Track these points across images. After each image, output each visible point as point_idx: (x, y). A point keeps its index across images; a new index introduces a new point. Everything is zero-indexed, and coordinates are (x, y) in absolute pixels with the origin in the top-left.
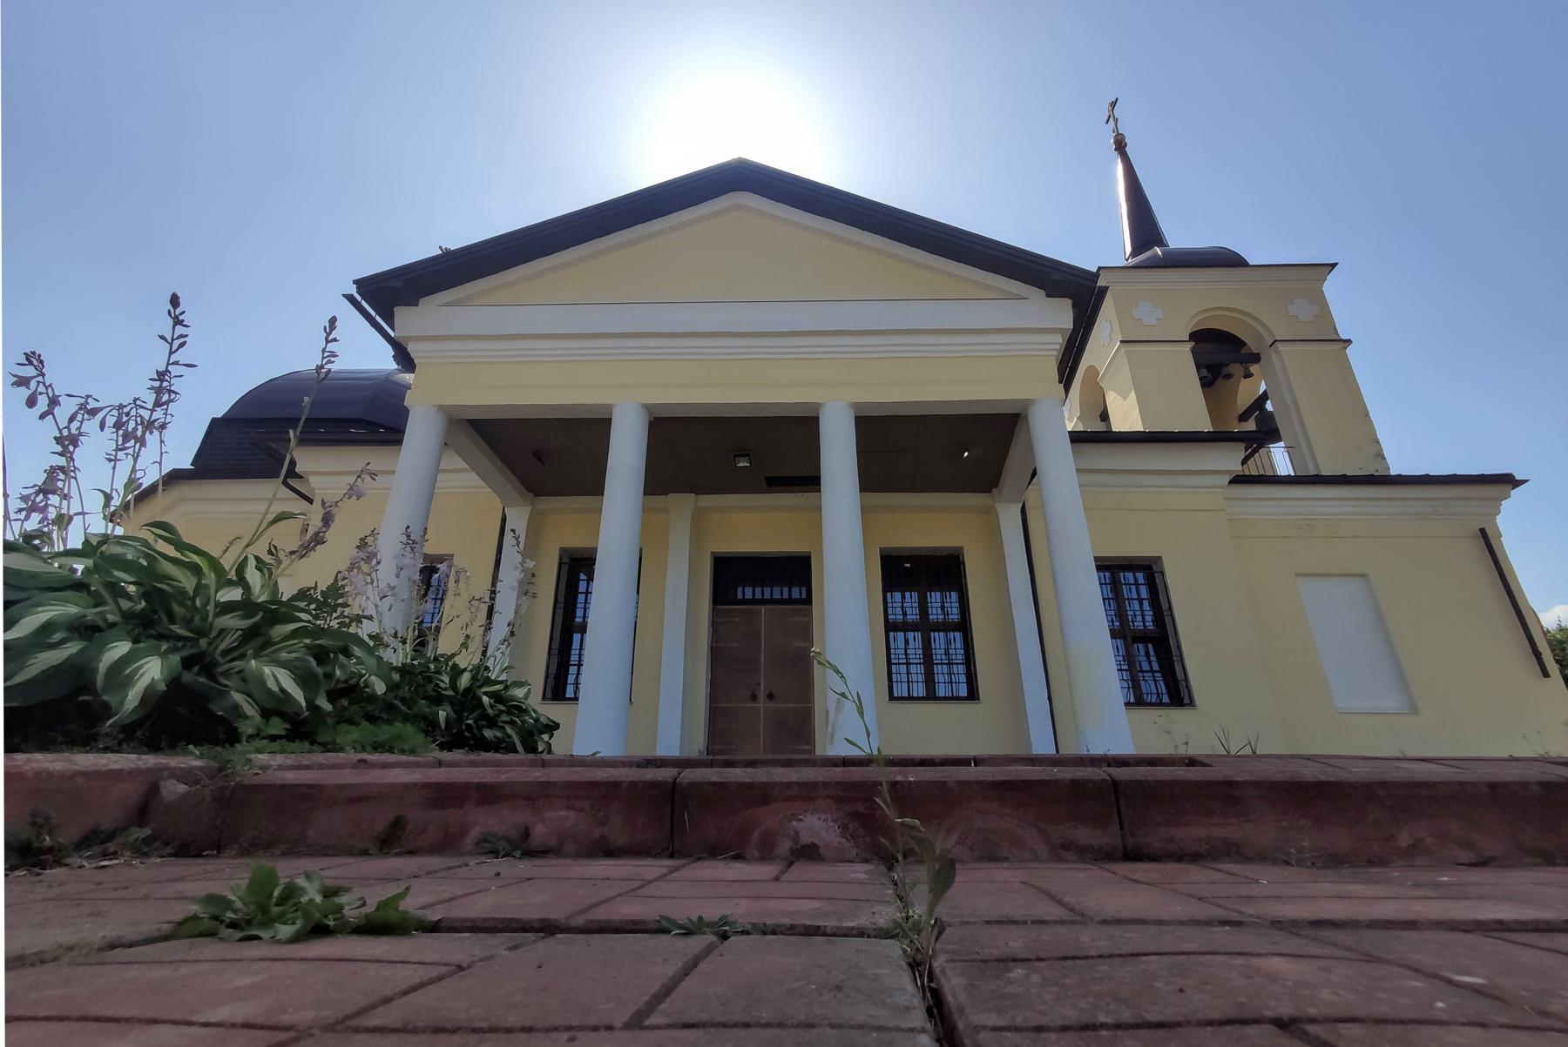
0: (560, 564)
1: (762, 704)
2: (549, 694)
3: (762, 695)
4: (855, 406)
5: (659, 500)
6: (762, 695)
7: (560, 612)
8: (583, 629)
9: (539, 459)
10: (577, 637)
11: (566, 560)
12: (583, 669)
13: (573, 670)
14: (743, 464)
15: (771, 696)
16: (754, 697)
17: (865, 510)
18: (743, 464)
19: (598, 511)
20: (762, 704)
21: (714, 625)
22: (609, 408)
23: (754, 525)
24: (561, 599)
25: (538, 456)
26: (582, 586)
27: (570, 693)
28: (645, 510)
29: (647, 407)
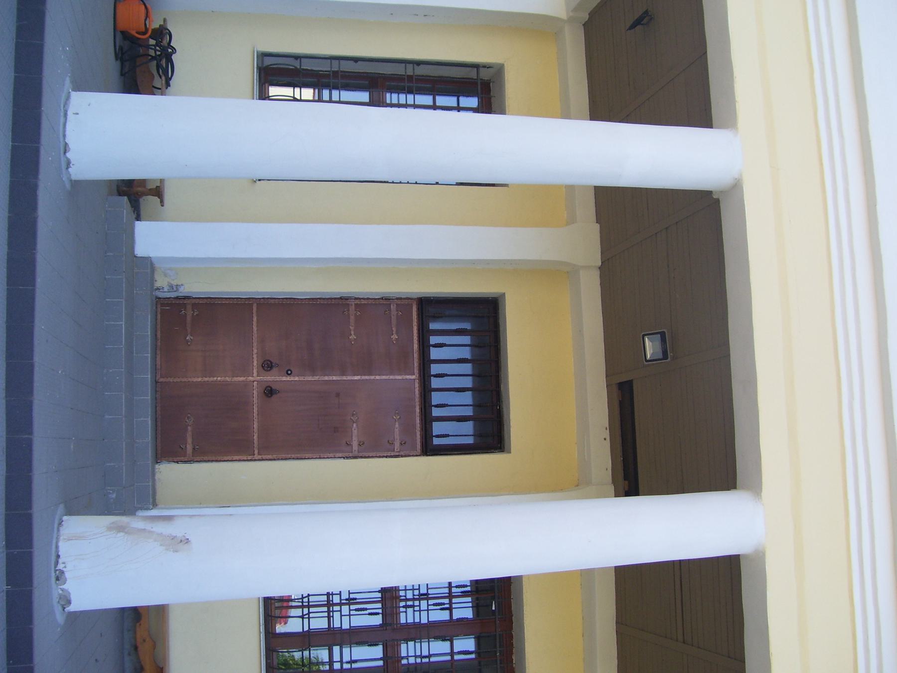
0: (476, 66)
1: (256, 378)
2: (268, 61)
3: (274, 378)
4: (759, 557)
5: (587, 209)
6: (274, 378)
7: (400, 70)
8: (376, 102)
9: (638, 22)
10: (364, 96)
11: (485, 75)
12: (454, 114)
13: (427, 100)
14: (651, 348)
15: (269, 392)
16: (267, 366)
17: (587, 575)
18: (651, 348)
19: (566, 114)
20: (256, 378)
21: (385, 301)
22: (730, 123)
23: (554, 367)
24: (420, 71)
25: (643, 20)
26: (466, 101)
27: (274, 91)
28: (571, 190)
29: (736, 187)
